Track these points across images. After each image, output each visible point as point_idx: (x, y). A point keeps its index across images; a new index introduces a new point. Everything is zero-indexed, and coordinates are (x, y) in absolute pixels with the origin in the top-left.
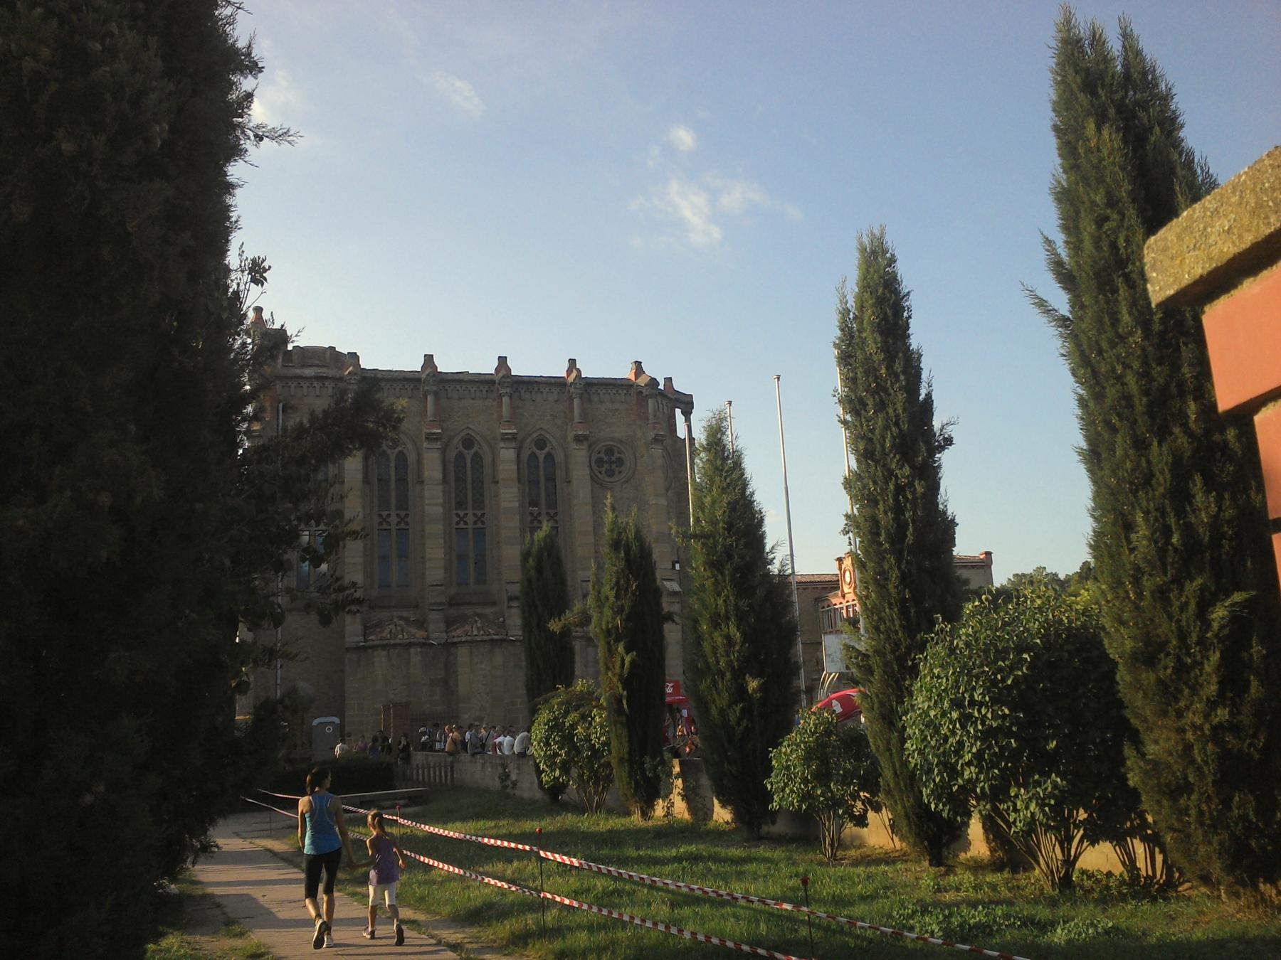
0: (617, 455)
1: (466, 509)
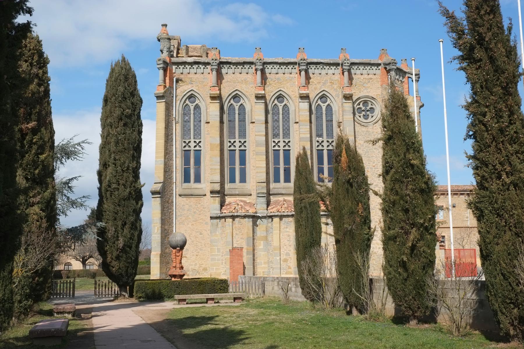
0: (370, 106)
1: (235, 138)
